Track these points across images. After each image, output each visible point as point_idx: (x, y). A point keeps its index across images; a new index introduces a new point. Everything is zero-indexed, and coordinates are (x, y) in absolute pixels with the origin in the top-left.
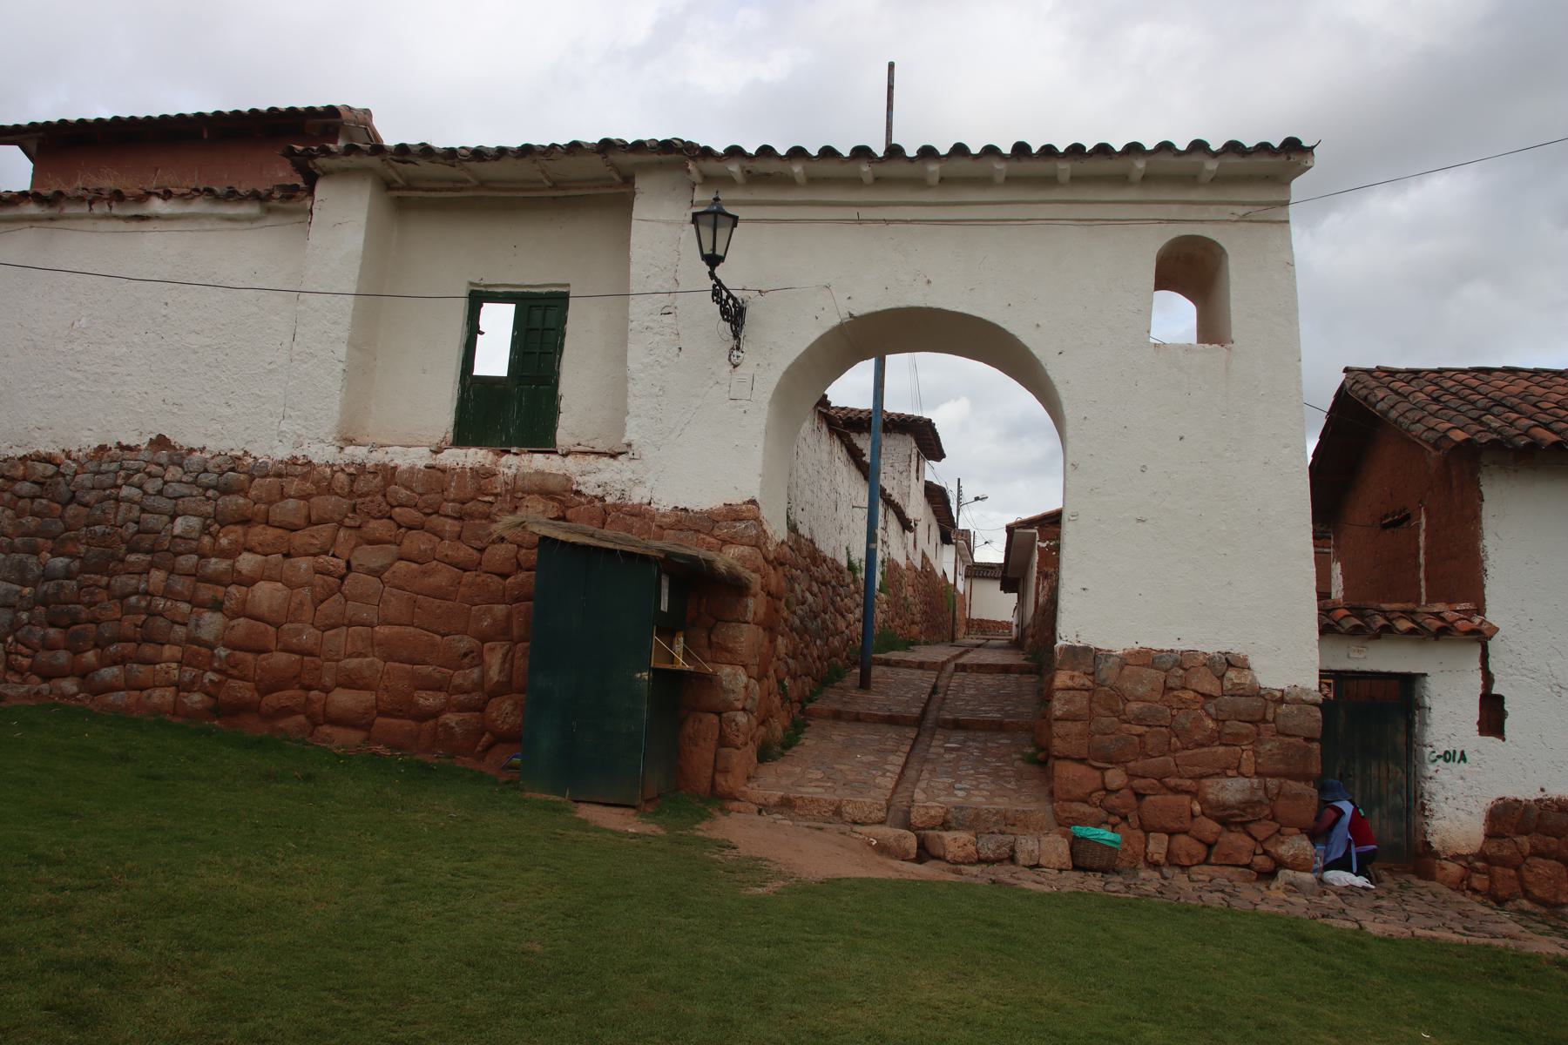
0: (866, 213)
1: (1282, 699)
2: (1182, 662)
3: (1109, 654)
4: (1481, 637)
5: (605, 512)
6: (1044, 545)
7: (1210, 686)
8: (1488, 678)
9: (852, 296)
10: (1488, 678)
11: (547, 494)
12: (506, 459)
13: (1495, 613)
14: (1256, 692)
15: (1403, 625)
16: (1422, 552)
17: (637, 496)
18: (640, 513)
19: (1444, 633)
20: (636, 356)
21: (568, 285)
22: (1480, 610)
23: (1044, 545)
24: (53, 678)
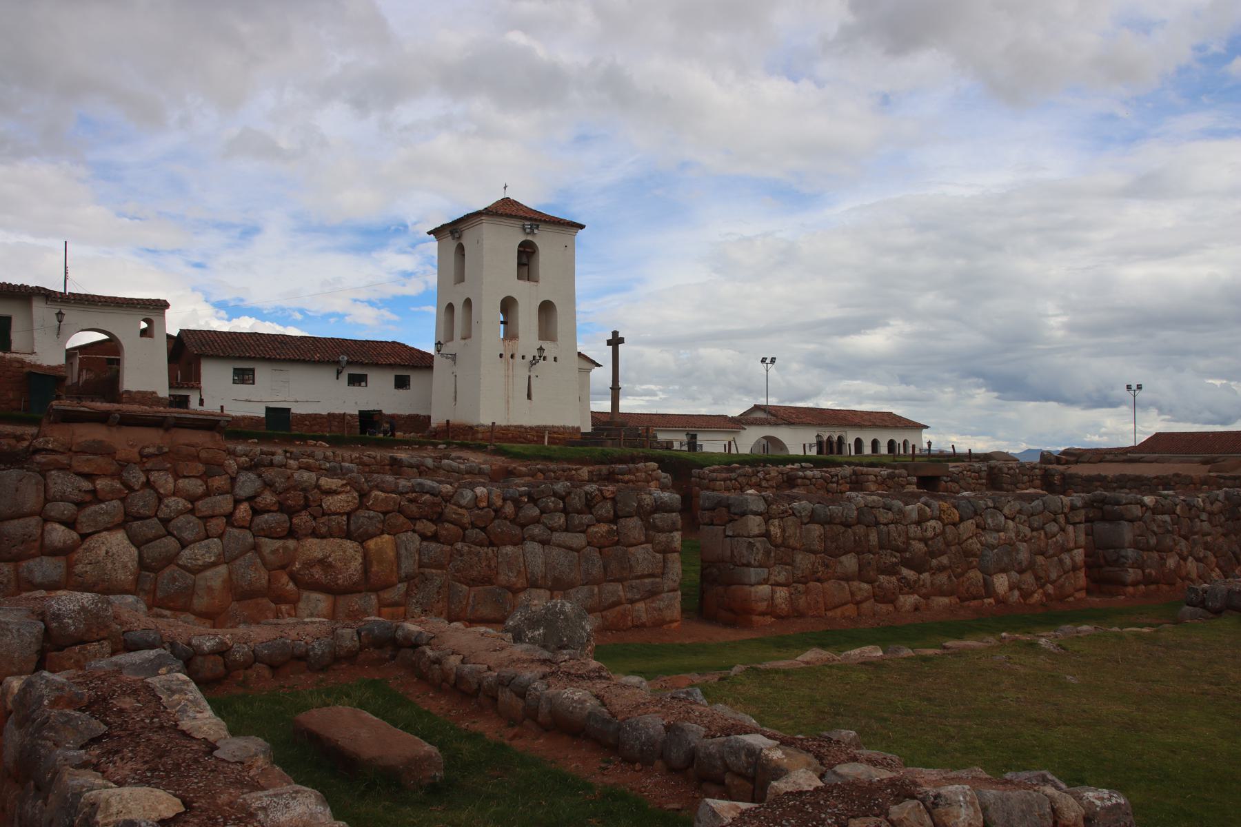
0: (508, 224)
1: (162, 398)
2: (145, 393)
3: (132, 391)
4: (199, 389)
5: (31, 365)
6: (81, 357)
7: (150, 397)
8: (201, 396)
9: (554, 355)
10: (201, 396)
11: (18, 362)
12: (7, 354)
13: (203, 384)
14: (158, 398)
15: (186, 386)
16: (1139, 629)
17: (38, 363)
18: (40, 366)
19: (192, 388)
20: (36, 335)
21: (804, 445)
22: (200, 383)
23: (81, 357)
24: (49, 521)
